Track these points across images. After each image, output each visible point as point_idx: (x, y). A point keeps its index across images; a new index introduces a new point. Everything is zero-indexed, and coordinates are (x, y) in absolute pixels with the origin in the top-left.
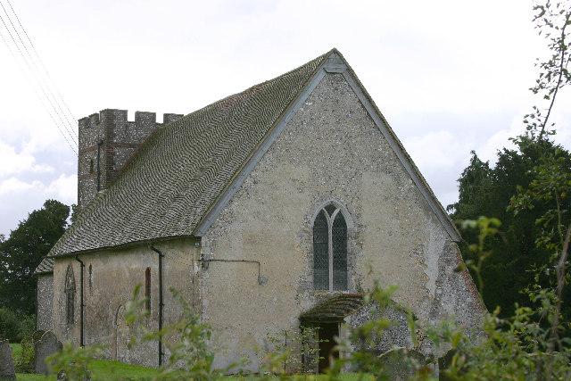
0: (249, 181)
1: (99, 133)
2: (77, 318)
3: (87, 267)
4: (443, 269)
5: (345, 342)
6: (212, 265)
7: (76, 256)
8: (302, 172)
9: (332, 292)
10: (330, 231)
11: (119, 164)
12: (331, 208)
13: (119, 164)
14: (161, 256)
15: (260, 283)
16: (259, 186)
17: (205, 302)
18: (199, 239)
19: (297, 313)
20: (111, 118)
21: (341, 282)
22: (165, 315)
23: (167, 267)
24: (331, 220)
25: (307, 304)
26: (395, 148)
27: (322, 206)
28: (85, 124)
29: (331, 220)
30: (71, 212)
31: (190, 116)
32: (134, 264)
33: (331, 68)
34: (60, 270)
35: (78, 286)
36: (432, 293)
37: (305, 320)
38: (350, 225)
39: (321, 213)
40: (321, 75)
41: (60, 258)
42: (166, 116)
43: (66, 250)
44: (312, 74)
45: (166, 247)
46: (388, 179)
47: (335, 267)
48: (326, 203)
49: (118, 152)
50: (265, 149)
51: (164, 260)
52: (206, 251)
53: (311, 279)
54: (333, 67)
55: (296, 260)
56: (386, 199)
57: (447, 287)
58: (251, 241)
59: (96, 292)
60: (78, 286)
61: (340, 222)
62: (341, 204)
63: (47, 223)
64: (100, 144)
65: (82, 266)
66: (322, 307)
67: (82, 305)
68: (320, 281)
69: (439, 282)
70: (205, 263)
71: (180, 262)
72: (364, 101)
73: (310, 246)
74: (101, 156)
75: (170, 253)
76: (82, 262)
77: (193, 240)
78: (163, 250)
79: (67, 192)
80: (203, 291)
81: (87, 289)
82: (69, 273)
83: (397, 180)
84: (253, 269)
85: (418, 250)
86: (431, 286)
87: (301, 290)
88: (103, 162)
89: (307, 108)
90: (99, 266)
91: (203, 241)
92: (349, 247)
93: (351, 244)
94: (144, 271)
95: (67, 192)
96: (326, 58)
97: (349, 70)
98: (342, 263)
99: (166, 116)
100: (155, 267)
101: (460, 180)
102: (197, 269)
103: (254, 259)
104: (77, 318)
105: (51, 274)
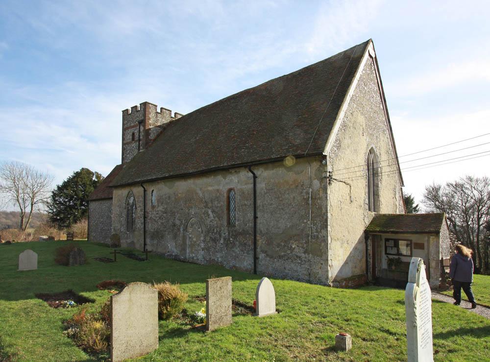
3: (149, 192)
60: (140, 205)
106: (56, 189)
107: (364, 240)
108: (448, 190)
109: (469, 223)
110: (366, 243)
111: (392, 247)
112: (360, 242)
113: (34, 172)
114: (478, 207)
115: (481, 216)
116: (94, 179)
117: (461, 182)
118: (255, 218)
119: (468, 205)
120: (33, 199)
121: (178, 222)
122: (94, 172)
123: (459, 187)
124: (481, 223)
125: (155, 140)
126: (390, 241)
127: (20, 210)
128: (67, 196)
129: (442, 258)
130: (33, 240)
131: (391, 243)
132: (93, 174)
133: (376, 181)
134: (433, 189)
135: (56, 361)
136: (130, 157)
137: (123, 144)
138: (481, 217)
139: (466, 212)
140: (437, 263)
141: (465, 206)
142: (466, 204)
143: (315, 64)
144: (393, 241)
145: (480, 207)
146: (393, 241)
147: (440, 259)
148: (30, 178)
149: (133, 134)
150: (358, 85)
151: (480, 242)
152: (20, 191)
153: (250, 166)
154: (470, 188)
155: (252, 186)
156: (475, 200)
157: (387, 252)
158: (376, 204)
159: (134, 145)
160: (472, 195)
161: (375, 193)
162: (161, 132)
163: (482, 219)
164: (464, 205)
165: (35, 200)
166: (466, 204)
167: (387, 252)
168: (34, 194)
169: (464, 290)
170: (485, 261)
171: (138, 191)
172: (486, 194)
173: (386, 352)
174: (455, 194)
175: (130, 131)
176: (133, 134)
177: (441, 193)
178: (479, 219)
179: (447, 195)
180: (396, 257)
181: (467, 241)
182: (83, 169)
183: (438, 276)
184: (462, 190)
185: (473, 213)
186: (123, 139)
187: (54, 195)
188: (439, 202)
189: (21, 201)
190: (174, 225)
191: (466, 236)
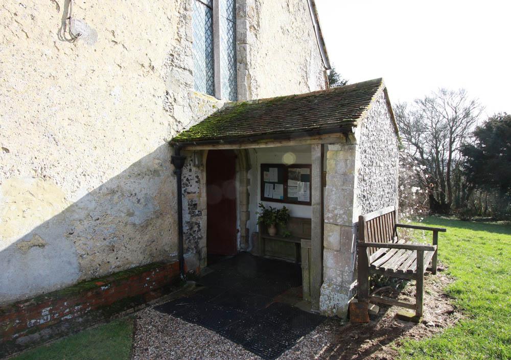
107: (172, 168)
108: (418, 108)
109: (439, 150)
110: (178, 173)
111: (274, 183)
112: (139, 171)
114: (451, 128)
115: (454, 139)
117: (431, 97)
119: (438, 126)
123: (427, 102)
124: (453, 149)
126: (271, 169)
129: (361, 218)
131: (273, 175)
133: (240, 29)
134: (397, 107)
138: (454, 141)
139: (436, 137)
140: (345, 236)
141: (435, 128)
142: (436, 125)
144: (276, 169)
145: (454, 128)
146: (276, 169)
147: (355, 220)
151: (451, 173)
154: (443, 104)
156: (448, 119)
157: (266, 196)
158: (239, 83)
160: (444, 113)
161: (239, 58)
163: (455, 144)
164: (434, 126)
166: (436, 125)
167: (266, 196)
169: (423, 272)
170: (456, 196)
172: (461, 111)
174: (424, 114)
177: (406, 112)
178: (451, 143)
179: (413, 114)
180: (279, 206)
181: (436, 172)
183: (347, 277)
184: (433, 107)
185: (444, 137)
188: (404, 123)
191: (434, 165)
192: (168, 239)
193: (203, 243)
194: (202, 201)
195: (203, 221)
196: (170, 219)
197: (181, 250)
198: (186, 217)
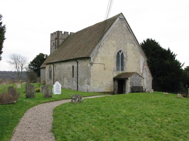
0: (102, 43)
1: (56, 36)
2: (52, 77)
3: (55, 66)
4: (143, 67)
5: (128, 86)
6: (93, 65)
7: (53, 63)
8: (114, 42)
9: (121, 72)
10: (120, 57)
11: (60, 44)
12: (120, 51)
13: (60, 44)
14: (78, 63)
15: (105, 69)
16: (105, 45)
17: (92, 74)
18: (90, 58)
19: (113, 77)
20: (58, 33)
21: (122, 69)
22: (79, 77)
23: (79, 65)
24: (120, 54)
25: (115, 75)
26: (134, 38)
27: (118, 51)
28: (52, 35)
29: (120, 54)
30: (45, 56)
31: (77, 33)
32: (69, 65)
33: (121, 17)
34: (47, 67)
35: (52, 70)
36: (141, 72)
37: (115, 79)
38: (125, 56)
39: (118, 52)
40: (118, 19)
41: (47, 64)
42: (71, 33)
43: (45, 63)
44: (116, 18)
45: (79, 60)
46: (133, 45)
47: (121, 66)
48: (119, 50)
49: (60, 40)
50: (106, 36)
51: (78, 63)
52: (92, 61)
53: (116, 68)
54: (121, 17)
55: (112, 64)
56: (132, 49)
57: (144, 71)
58: (102, 58)
59: (58, 72)
60: (52, 70)
61: (122, 54)
62: (123, 50)
63: (40, 60)
64: (56, 39)
65: (54, 66)
66: (119, 75)
67: (54, 75)
68: (118, 69)
69: (143, 70)
70: (92, 64)
71: (83, 64)
72: (128, 26)
73: (116, 60)
74: (56, 41)
75: (79, 61)
76: (77, 62)
77: (89, 58)
78: (79, 61)
79: (47, 52)
80: (91, 71)
81: (55, 71)
82: (50, 67)
83: (135, 45)
84: (103, 66)
85: (139, 62)
86: (141, 70)
87: (114, 71)
88: (56, 43)
89: (115, 26)
90: (58, 66)
91: (91, 58)
92: (124, 61)
93: (125, 60)
94: (72, 66)
95: (47, 52)
96: (119, 15)
97: (124, 18)
98: (122, 65)
99: (71, 33)
100: (75, 65)
101: (158, 43)
102: (89, 65)
103: (103, 63)
104: (52, 77)
105: (45, 68)
106: (30, 63)
113: (22, 56)
116: (45, 57)
118: (78, 75)
120: (22, 67)
121: (62, 76)
122: (45, 54)
125: (61, 45)
127: (17, 71)
128: (34, 66)
130: (99, 44)
132: (44, 55)
135: (140, 140)
136: (53, 51)
137: (51, 47)
143: (93, 25)
148: (21, 58)
149: (54, 43)
150: (54, 60)
152: (17, 64)
153: (76, 60)
155: (77, 65)
159: (54, 47)
162: (64, 42)
165: (23, 67)
168: (22, 65)
171: (52, 66)
173: (147, 110)
175: (53, 42)
176: (54, 43)
182: (40, 54)
186: (51, 45)
187: (30, 65)
189: (18, 68)
190: (61, 77)
192: (113, 89)
193: (117, 91)
194: (117, 85)
195: (117, 88)
196: (113, 87)
197: (114, 91)
198: (115, 87)
